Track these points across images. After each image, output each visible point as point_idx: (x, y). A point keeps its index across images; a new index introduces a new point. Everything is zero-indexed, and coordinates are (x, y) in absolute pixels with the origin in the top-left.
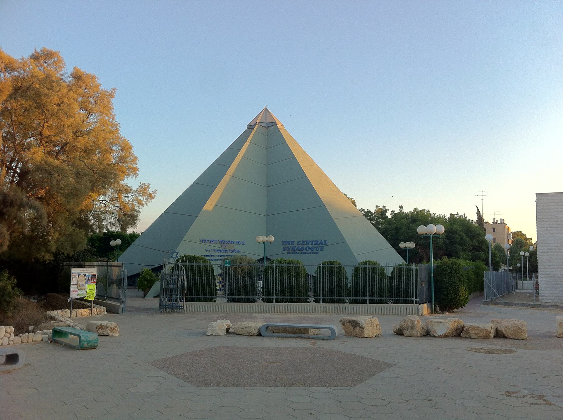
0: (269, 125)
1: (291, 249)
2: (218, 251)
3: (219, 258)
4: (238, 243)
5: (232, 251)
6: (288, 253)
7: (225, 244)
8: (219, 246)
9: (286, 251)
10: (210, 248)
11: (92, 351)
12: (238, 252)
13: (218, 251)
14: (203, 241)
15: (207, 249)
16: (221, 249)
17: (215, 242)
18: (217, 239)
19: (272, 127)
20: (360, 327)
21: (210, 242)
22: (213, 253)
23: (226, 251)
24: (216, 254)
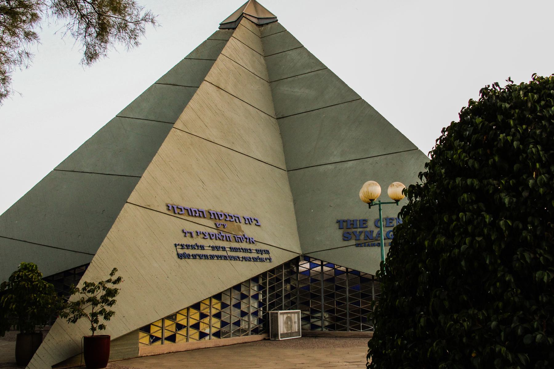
0: (262, 22)
1: (362, 237)
2: (211, 236)
3: (216, 253)
4: (249, 221)
5: (238, 240)
6: (357, 245)
7: (223, 222)
8: (211, 223)
9: (353, 242)
10: (192, 228)
11: (110, 272)
12: (251, 241)
13: (211, 236)
14: (174, 210)
15: (187, 229)
16: (216, 232)
17: (201, 214)
18: (204, 208)
19: (269, 26)
20: (261, 331)
21: (190, 212)
22: (200, 241)
23: (228, 239)
24: (207, 243)
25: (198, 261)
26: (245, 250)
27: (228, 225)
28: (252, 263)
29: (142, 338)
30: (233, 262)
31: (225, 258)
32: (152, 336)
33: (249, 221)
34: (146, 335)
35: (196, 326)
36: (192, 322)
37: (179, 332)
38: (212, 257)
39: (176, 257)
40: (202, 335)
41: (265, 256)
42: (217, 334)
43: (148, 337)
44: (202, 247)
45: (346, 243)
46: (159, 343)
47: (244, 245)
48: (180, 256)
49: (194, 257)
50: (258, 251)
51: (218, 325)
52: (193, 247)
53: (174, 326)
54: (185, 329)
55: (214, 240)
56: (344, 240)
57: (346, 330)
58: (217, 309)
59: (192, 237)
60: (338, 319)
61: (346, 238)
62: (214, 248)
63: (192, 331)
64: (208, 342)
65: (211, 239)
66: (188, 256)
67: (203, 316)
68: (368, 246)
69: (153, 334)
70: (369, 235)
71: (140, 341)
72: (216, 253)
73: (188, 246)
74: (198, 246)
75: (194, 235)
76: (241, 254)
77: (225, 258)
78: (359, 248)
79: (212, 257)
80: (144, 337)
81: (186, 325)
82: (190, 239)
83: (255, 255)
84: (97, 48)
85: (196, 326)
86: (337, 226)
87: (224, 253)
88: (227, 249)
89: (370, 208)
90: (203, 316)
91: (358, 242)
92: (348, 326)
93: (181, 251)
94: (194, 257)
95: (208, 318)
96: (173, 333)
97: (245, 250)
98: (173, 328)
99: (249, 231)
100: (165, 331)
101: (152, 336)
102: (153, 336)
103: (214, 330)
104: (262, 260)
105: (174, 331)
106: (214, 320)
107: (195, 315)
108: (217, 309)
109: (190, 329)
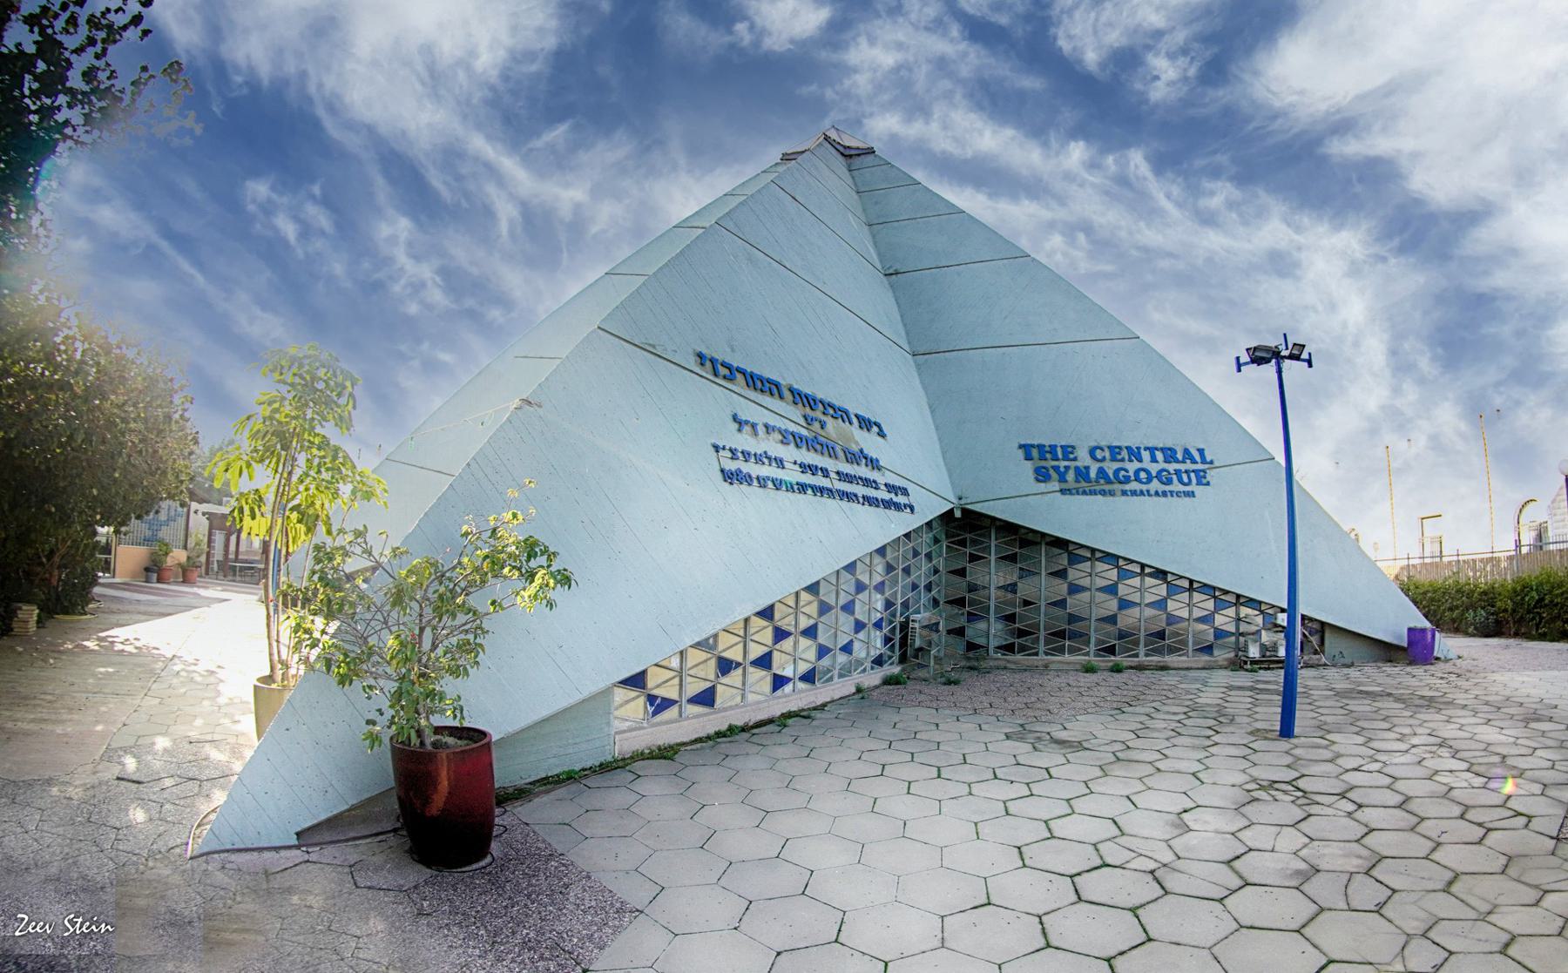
2: (798, 441)
3: (807, 479)
4: (866, 424)
6: (1063, 491)
8: (796, 413)
9: (1054, 485)
12: (874, 464)
23: (833, 455)
24: (789, 453)
25: (770, 491)
26: (867, 482)
27: (830, 422)
28: (881, 511)
29: (621, 706)
30: (845, 504)
31: (830, 492)
32: (651, 699)
33: (866, 424)
34: (633, 694)
35: (764, 662)
36: (756, 651)
37: (724, 680)
38: (803, 488)
39: (719, 476)
40: (779, 682)
41: (901, 499)
42: (809, 677)
43: (642, 700)
44: (780, 463)
45: (1042, 487)
46: (672, 713)
47: (863, 471)
48: (729, 477)
49: (762, 482)
50: (891, 488)
51: (811, 655)
52: (759, 459)
53: (713, 663)
54: (740, 671)
55: (804, 450)
56: (1038, 480)
57: (1036, 654)
58: (809, 616)
59: (756, 434)
60: (1022, 633)
61: (1042, 475)
62: (806, 468)
63: (756, 674)
64: (796, 697)
65: (797, 446)
66: (745, 479)
67: (780, 635)
68: (1084, 493)
69: (655, 692)
70: (1082, 474)
71: (617, 713)
72: (807, 479)
73: (746, 455)
74: (769, 458)
75: (761, 429)
76: (861, 490)
77: (830, 492)
78: (1068, 497)
79: (803, 488)
80: (627, 702)
81: (740, 659)
82: (751, 440)
83: (883, 494)
84: (318, 430)
85: (764, 662)
86: (1021, 453)
87: (825, 483)
88: (833, 475)
89: (1021, 446)
90: (780, 635)
91: (1064, 486)
92: (1042, 648)
93: (732, 466)
94: (762, 482)
95: (791, 638)
96: (708, 685)
97: (867, 482)
98: (711, 669)
99: (867, 442)
100: (689, 679)
101: (651, 699)
102: (655, 697)
103: (803, 668)
104: (898, 507)
105: (712, 677)
106: (804, 642)
107: (763, 634)
108: (809, 616)
109: (751, 669)
